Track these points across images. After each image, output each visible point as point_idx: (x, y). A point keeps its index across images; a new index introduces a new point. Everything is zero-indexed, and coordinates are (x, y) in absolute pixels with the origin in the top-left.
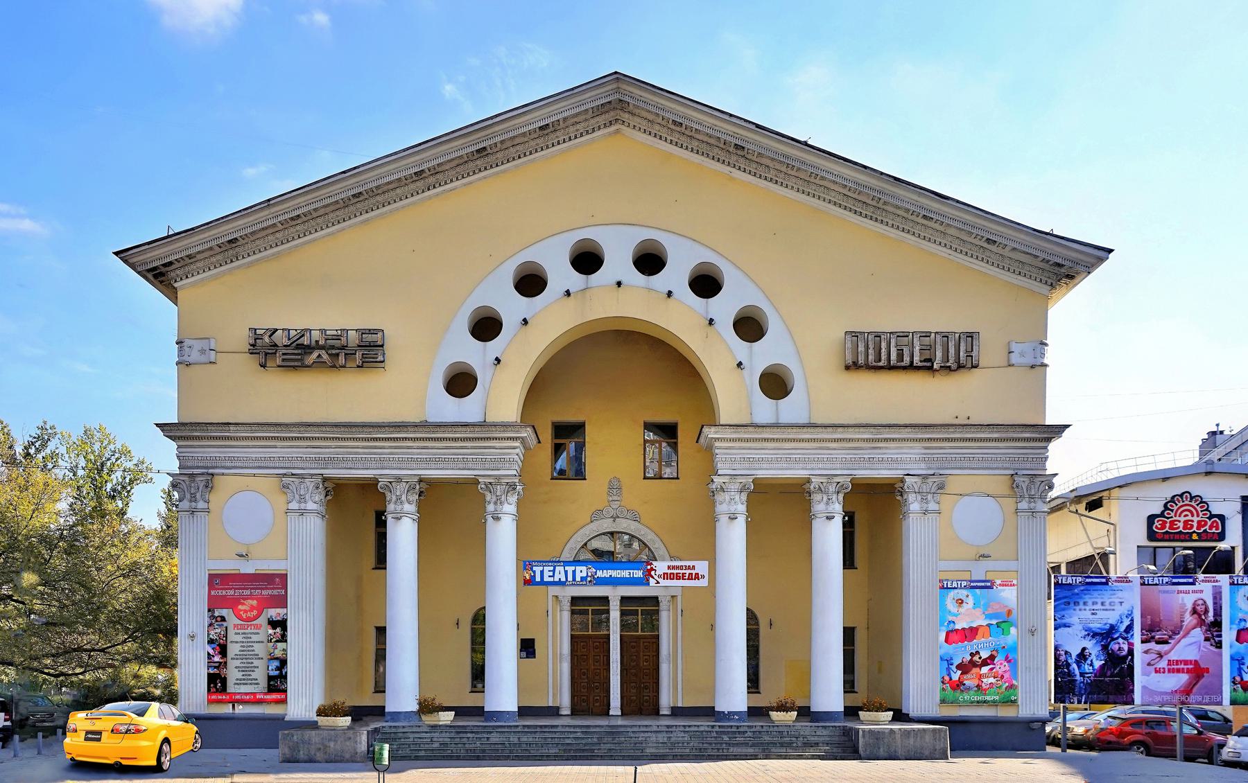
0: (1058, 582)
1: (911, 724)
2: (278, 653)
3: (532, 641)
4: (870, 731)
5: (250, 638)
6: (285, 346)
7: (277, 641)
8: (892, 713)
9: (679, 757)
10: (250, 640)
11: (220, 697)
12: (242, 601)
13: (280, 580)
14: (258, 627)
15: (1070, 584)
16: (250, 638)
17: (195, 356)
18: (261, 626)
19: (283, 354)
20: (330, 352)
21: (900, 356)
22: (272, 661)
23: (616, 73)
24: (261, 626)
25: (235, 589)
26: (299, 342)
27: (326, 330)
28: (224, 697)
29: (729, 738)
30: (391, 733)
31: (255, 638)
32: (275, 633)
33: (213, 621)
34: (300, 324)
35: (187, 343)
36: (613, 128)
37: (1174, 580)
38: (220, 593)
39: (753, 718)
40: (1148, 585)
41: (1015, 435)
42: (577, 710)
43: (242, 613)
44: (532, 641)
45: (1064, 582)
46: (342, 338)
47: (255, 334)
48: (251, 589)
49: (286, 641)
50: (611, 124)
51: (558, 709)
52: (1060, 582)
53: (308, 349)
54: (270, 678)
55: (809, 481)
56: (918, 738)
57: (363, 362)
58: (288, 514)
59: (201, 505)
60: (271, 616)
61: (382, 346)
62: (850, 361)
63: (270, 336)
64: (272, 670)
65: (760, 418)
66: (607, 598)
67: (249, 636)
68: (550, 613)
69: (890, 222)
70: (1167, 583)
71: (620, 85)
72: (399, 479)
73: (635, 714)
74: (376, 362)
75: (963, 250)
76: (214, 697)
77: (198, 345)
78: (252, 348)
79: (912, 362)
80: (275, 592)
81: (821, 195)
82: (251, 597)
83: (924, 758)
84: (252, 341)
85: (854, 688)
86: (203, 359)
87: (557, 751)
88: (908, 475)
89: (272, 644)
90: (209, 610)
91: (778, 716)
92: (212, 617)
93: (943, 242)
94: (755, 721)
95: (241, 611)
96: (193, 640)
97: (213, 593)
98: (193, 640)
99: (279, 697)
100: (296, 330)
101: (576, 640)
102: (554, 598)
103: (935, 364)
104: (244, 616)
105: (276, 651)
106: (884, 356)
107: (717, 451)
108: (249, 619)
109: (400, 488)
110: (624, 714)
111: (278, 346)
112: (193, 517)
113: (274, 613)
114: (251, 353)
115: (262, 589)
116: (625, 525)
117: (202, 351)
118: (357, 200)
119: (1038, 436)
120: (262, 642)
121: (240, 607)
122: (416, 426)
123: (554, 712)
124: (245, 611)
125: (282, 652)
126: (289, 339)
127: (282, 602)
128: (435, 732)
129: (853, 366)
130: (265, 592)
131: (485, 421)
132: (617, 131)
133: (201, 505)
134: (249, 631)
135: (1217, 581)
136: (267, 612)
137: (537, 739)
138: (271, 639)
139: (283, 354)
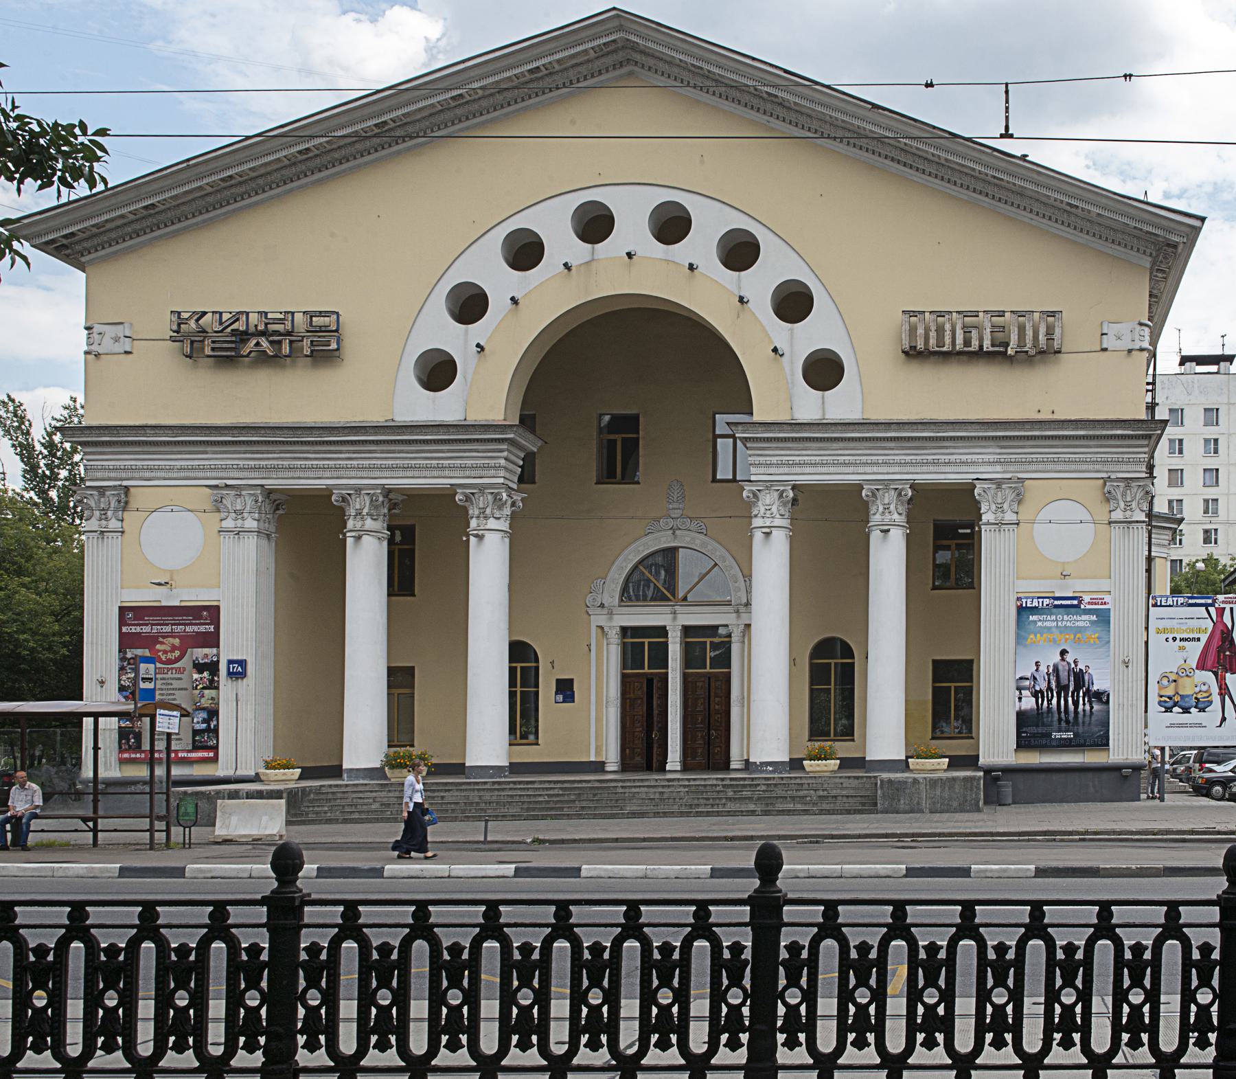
0: (1022, 605)
1: (856, 770)
2: (205, 703)
3: (570, 682)
4: (890, 781)
5: (171, 684)
6: (216, 332)
7: (204, 688)
8: (947, 760)
9: (661, 815)
10: (171, 687)
11: (133, 756)
12: (161, 639)
13: (212, 613)
14: (180, 671)
15: (1035, 607)
16: (171, 684)
17: (107, 345)
18: (184, 669)
19: (213, 342)
20: (271, 338)
21: (967, 342)
22: (197, 712)
23: (614, 9)
24: (184, 669)
25: (153, 625)
26: (234, 326)
27: (266, 313)
28: (138, 755)
29: (734, 792)
30: (328, 793)
31: (176, 684)
32: (201, 678)
33: (125, 664)
34: (229, 307)
35: (97, 328)
36: (624, 70)
37: (1191, 601)
38: (134, 629)
39: (844, 770)
40: (1161, 606)
41: (1104, 432)
42: (626, 765)
43: (160, 654)
44: (570, 682)
45: (1028, 605)
46: (286, 322)
47: (179, 318)
48: (172, 625)
49: (217, 688)
50: (621, 66)
51: (603, 763)
52: (1024, 605)
53: (243, 336)
54: (196, 732)
55: (860, 487)
56: (947, 788)
57: (312, 351)
58: (221, 533)
59: (114, 524)
60: (197, 658)
61: (337, 331)
62: (907, 347)
63: (197, 320)
64: (198, 722)
65: (803, 415)
66: (664, 628)
67: (170, 681)
68: (593, 647)
69: (959, 182)
70: (1182, 604)
71: (623, 23)
72: (358, 490)
73: (702, 769)
74: (329, 350)
75: (1047, 213)
76: (126, 755)
77: (110, 331)
78: (175, 334)
79: (981, 347)
80: (202, 629)
81: (875, 149)
82: (172, 635)
83: (952, 810)
84: (175, 327)
85: (971, 733)
86: (118, 348)
87: (519, 810)
88: (977, 479)
89: (198, 692)
90: (120, 651)
91: (811, 766)
92: (122, 659)
93: (1023, 205)
94: (712, 774)
95: (159, 651)
96: (102, 687)
97: (124, 629)
98: (102, 687)
99: (205, 754)
100: (230, 313)
101: (628, 680)
102: (599, 630)
103: (1009, 349)
104: (163, 658)
105: (203, 700)
106: (948, 340)
107: (521, 463)
108: (170, 662)
109: (356, 504)
110: (686, 768)
111: (207, 332)
112: (103, 538)
113: (200, 653)
114: (174, 341)
115: (185, 625)
116: (688, 539)
117: (116, 339)
118: (306, 156)
119: (1132, 433)
120: (186, 689)
121: (158, 647)
122: (377, 429)
123: (599, 767)
124: (165, 652)
125: (211, 702)
126: (221, 324)
127: (212, 640)
128: (381, 791)
129: (913, 354)
130: (189, 629)
131: (465, 420)
132: (631, 74)
133: (114, 524)
134: (170, 675)
135: (1105, 603)
136: (192, 654)
137: (502, 798)
138: (197, 686)
139: (213, 342)
